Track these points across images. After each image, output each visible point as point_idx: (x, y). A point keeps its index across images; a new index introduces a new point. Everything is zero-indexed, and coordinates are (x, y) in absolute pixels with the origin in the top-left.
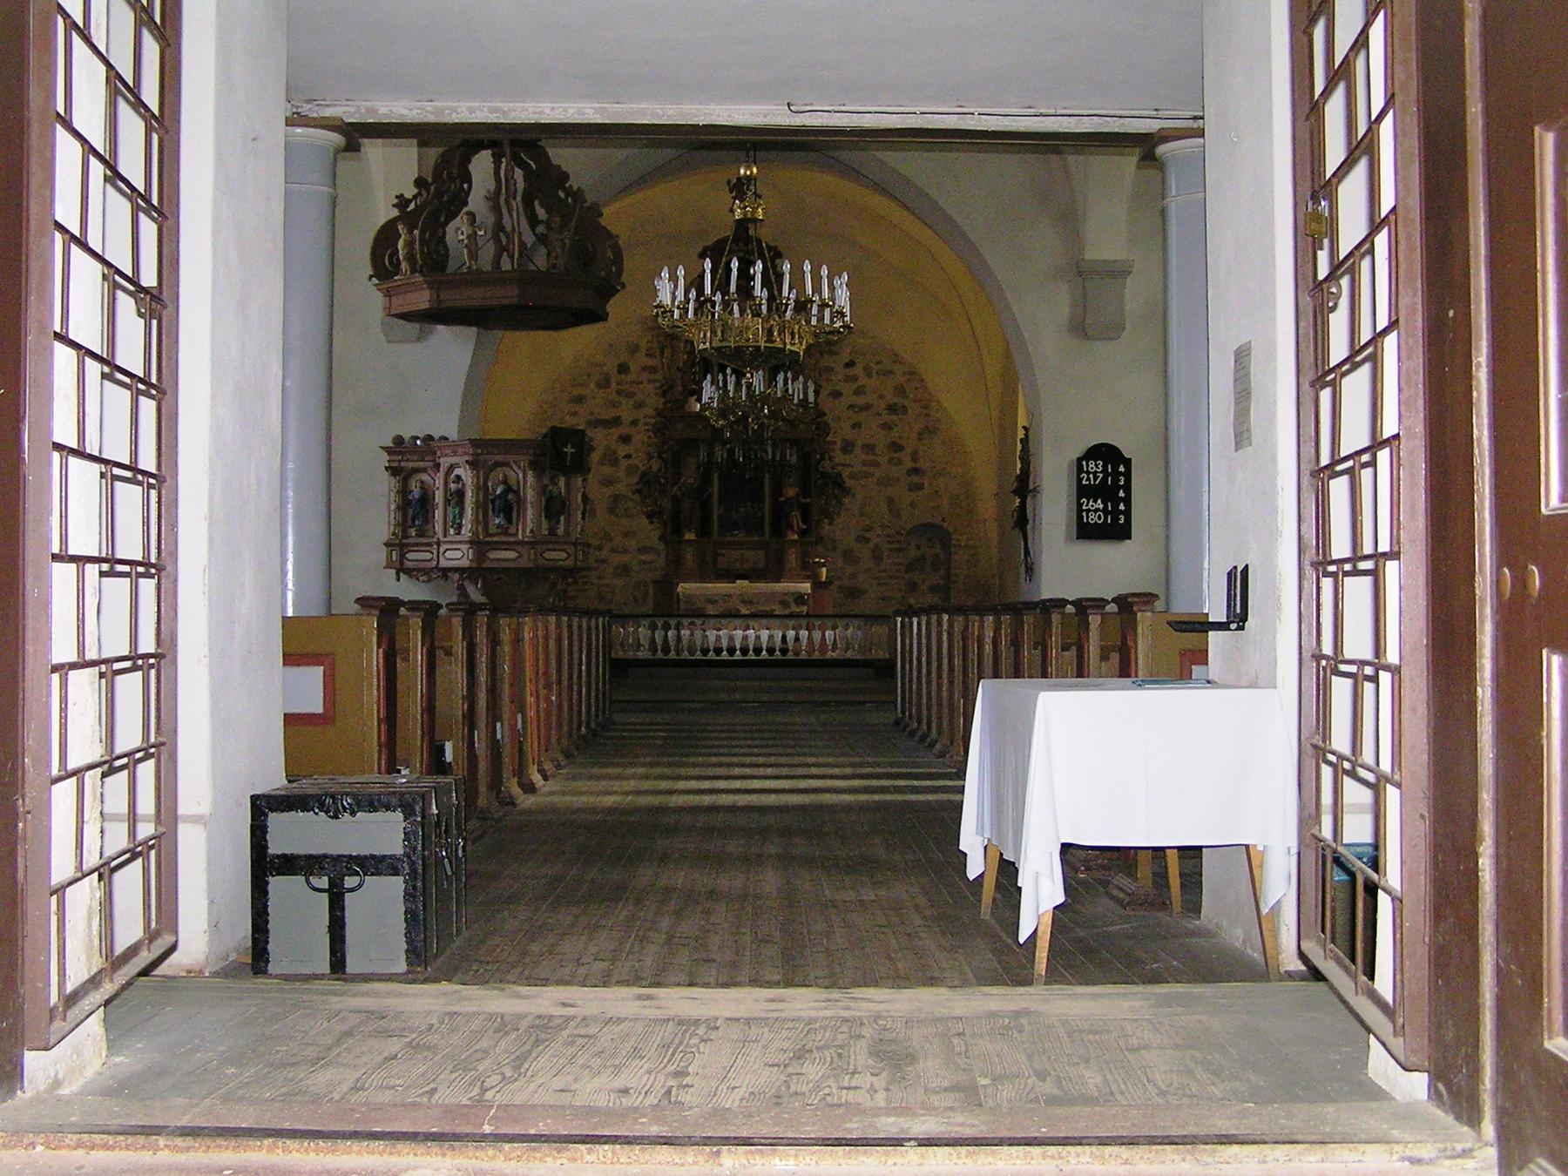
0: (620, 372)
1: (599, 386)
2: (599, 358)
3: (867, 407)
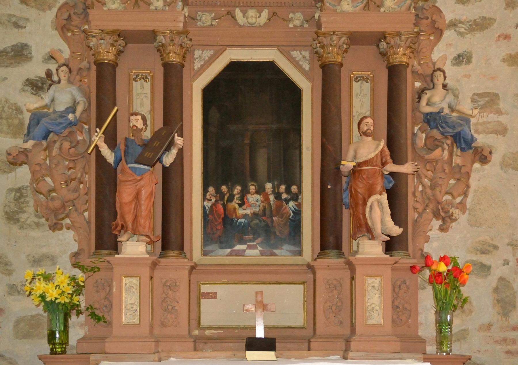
3: (481, 25)
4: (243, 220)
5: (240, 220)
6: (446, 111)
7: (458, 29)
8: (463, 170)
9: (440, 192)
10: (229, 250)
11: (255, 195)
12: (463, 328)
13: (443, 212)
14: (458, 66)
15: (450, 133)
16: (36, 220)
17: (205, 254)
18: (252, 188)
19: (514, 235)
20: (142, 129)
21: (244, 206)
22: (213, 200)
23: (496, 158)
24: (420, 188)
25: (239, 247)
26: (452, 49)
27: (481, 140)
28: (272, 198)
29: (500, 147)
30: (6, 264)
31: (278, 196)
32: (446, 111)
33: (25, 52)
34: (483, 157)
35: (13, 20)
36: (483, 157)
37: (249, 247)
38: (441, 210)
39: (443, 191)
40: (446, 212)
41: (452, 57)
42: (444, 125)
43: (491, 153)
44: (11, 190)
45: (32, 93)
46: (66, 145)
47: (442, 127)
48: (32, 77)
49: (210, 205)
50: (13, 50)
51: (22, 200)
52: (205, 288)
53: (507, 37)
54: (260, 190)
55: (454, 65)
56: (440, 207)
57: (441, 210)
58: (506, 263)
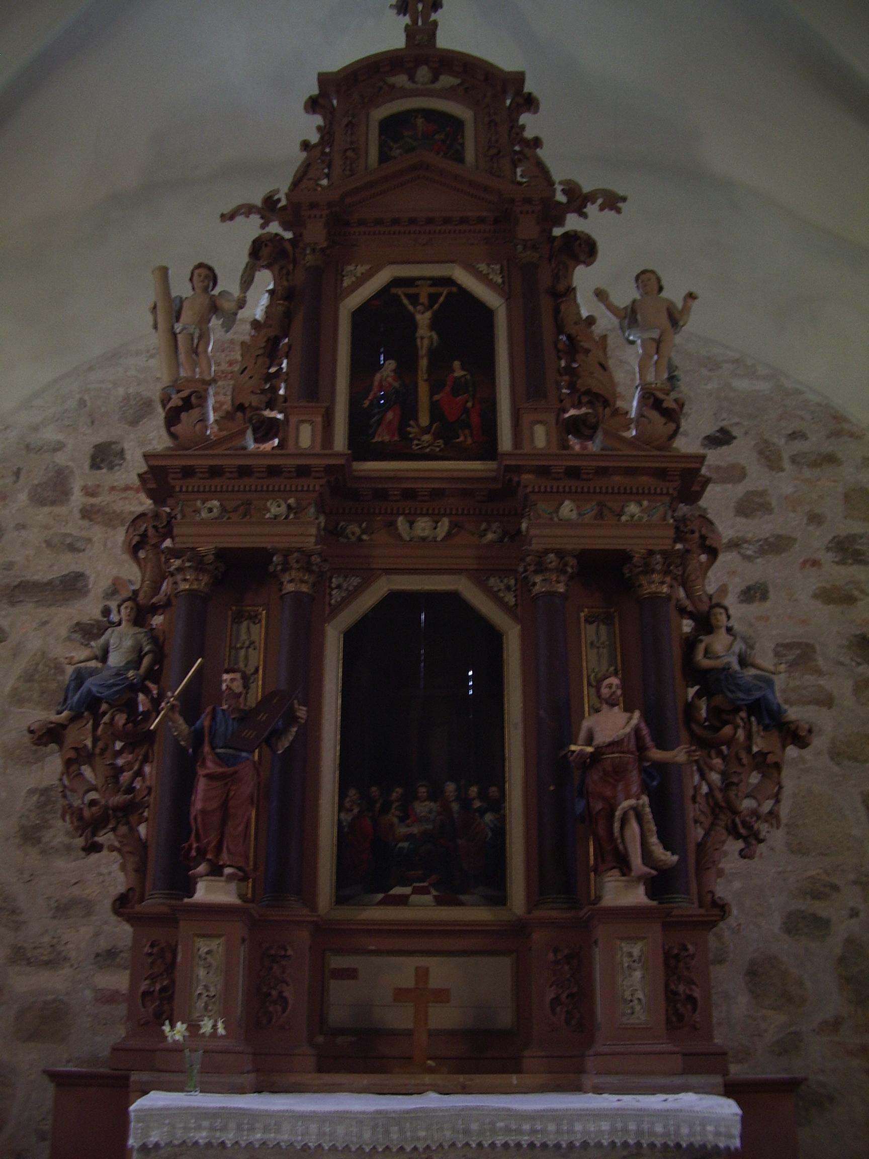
0: (95, 465)
1: (38, 499)
2: (50, 434)
3: (775, 546)
4: (405, 845)
5: (401, 845)
6: (736, 666)
7: (742, 551)
8: (771, 759)
9: (737, 795)
10: (381, 896)
11: (427, 803)
12: (793, 1029)
13: (744, 827)
14: (749, 603)
15: (743, 700)
16: (66, 840)
17: (341, 900)
18: (422, 790)
19: (862, 866)
20: (240, 694)
21: (409, 821)
22: (356, 811)
23: (819, 742)
24: (705, 789)
25: (398, 890)
26: (737, 580)
27: (793, 713)
28: (455, 806)
29: (826, 725)
30: (13, 912)
31: (466, 803)
32: (736, 666)
33: (79, 585)
34: (796, 736)
35: (69, 540)
36: (796, 736)
37: (416, 891)
38: (740, 826)
39: (740, 794)
40: (749, 827)
41: (738, 590)
42: (733, 688)
43: (810, 731)
44: (32, 792)
45: (82, 644)
46: (121, 719)
47: (732, 692)
48: (85, 620)
49: (349, 819)
50: (61, 581)
51: (48, 808)
52: (337, 962)
53: (815, 563)
54: (436, 794)
55: (742, 601)
56: (738, 820)
57: (740, 826)
58: (854, 913)
